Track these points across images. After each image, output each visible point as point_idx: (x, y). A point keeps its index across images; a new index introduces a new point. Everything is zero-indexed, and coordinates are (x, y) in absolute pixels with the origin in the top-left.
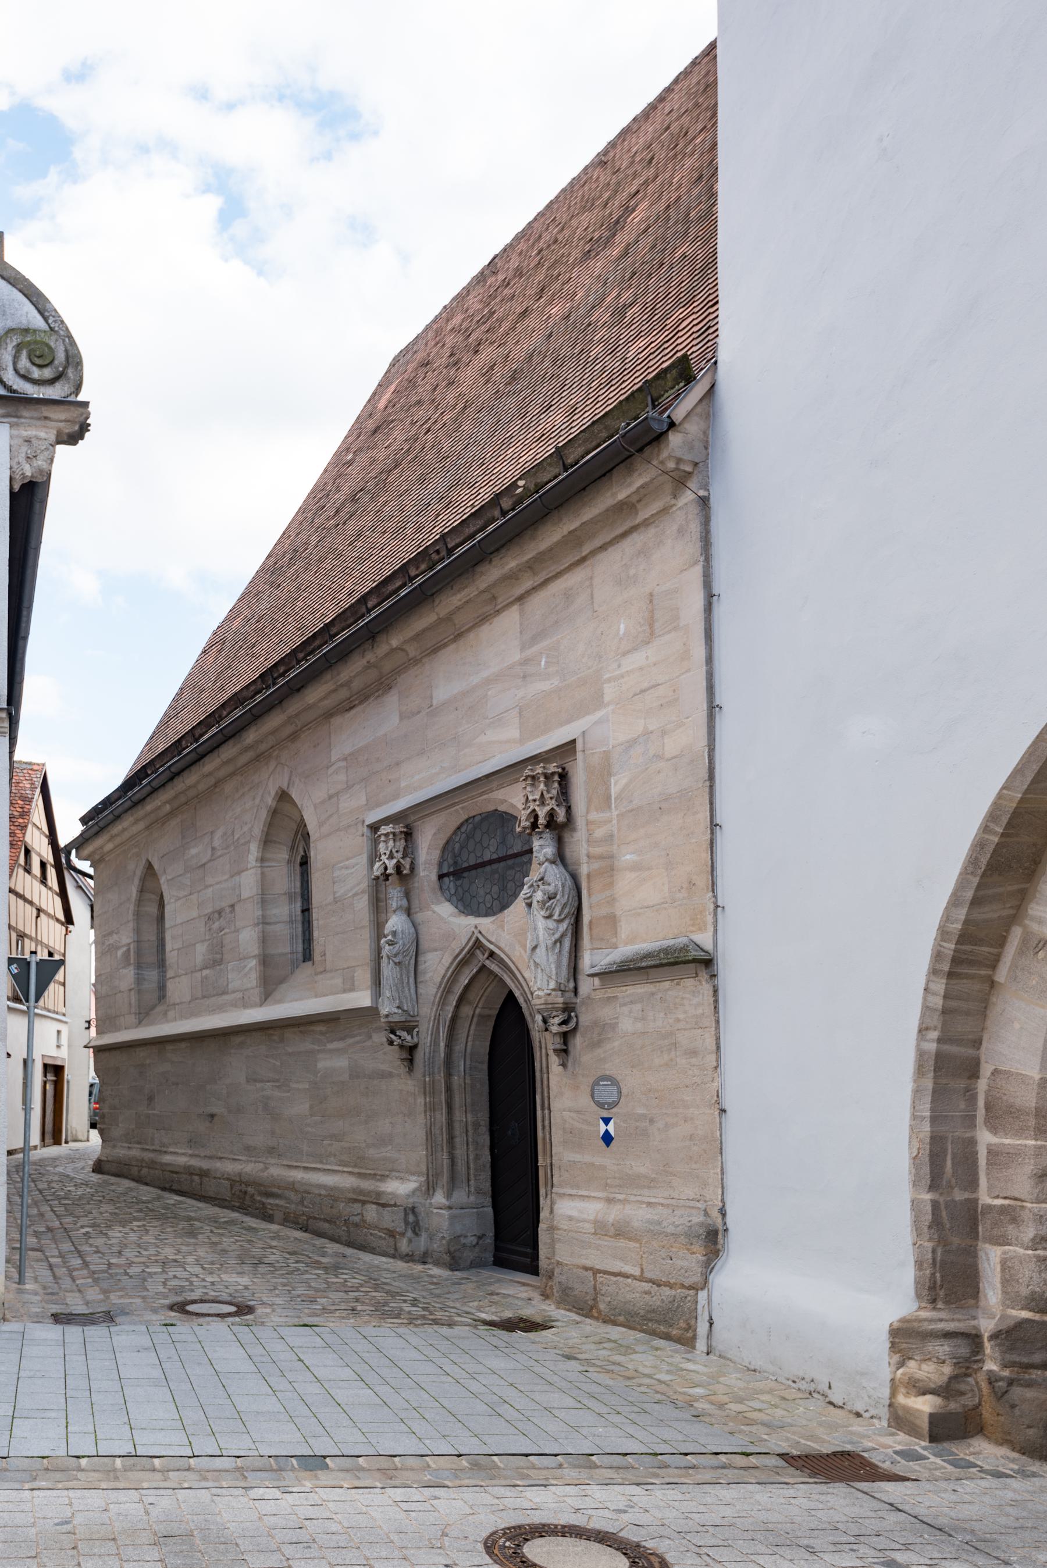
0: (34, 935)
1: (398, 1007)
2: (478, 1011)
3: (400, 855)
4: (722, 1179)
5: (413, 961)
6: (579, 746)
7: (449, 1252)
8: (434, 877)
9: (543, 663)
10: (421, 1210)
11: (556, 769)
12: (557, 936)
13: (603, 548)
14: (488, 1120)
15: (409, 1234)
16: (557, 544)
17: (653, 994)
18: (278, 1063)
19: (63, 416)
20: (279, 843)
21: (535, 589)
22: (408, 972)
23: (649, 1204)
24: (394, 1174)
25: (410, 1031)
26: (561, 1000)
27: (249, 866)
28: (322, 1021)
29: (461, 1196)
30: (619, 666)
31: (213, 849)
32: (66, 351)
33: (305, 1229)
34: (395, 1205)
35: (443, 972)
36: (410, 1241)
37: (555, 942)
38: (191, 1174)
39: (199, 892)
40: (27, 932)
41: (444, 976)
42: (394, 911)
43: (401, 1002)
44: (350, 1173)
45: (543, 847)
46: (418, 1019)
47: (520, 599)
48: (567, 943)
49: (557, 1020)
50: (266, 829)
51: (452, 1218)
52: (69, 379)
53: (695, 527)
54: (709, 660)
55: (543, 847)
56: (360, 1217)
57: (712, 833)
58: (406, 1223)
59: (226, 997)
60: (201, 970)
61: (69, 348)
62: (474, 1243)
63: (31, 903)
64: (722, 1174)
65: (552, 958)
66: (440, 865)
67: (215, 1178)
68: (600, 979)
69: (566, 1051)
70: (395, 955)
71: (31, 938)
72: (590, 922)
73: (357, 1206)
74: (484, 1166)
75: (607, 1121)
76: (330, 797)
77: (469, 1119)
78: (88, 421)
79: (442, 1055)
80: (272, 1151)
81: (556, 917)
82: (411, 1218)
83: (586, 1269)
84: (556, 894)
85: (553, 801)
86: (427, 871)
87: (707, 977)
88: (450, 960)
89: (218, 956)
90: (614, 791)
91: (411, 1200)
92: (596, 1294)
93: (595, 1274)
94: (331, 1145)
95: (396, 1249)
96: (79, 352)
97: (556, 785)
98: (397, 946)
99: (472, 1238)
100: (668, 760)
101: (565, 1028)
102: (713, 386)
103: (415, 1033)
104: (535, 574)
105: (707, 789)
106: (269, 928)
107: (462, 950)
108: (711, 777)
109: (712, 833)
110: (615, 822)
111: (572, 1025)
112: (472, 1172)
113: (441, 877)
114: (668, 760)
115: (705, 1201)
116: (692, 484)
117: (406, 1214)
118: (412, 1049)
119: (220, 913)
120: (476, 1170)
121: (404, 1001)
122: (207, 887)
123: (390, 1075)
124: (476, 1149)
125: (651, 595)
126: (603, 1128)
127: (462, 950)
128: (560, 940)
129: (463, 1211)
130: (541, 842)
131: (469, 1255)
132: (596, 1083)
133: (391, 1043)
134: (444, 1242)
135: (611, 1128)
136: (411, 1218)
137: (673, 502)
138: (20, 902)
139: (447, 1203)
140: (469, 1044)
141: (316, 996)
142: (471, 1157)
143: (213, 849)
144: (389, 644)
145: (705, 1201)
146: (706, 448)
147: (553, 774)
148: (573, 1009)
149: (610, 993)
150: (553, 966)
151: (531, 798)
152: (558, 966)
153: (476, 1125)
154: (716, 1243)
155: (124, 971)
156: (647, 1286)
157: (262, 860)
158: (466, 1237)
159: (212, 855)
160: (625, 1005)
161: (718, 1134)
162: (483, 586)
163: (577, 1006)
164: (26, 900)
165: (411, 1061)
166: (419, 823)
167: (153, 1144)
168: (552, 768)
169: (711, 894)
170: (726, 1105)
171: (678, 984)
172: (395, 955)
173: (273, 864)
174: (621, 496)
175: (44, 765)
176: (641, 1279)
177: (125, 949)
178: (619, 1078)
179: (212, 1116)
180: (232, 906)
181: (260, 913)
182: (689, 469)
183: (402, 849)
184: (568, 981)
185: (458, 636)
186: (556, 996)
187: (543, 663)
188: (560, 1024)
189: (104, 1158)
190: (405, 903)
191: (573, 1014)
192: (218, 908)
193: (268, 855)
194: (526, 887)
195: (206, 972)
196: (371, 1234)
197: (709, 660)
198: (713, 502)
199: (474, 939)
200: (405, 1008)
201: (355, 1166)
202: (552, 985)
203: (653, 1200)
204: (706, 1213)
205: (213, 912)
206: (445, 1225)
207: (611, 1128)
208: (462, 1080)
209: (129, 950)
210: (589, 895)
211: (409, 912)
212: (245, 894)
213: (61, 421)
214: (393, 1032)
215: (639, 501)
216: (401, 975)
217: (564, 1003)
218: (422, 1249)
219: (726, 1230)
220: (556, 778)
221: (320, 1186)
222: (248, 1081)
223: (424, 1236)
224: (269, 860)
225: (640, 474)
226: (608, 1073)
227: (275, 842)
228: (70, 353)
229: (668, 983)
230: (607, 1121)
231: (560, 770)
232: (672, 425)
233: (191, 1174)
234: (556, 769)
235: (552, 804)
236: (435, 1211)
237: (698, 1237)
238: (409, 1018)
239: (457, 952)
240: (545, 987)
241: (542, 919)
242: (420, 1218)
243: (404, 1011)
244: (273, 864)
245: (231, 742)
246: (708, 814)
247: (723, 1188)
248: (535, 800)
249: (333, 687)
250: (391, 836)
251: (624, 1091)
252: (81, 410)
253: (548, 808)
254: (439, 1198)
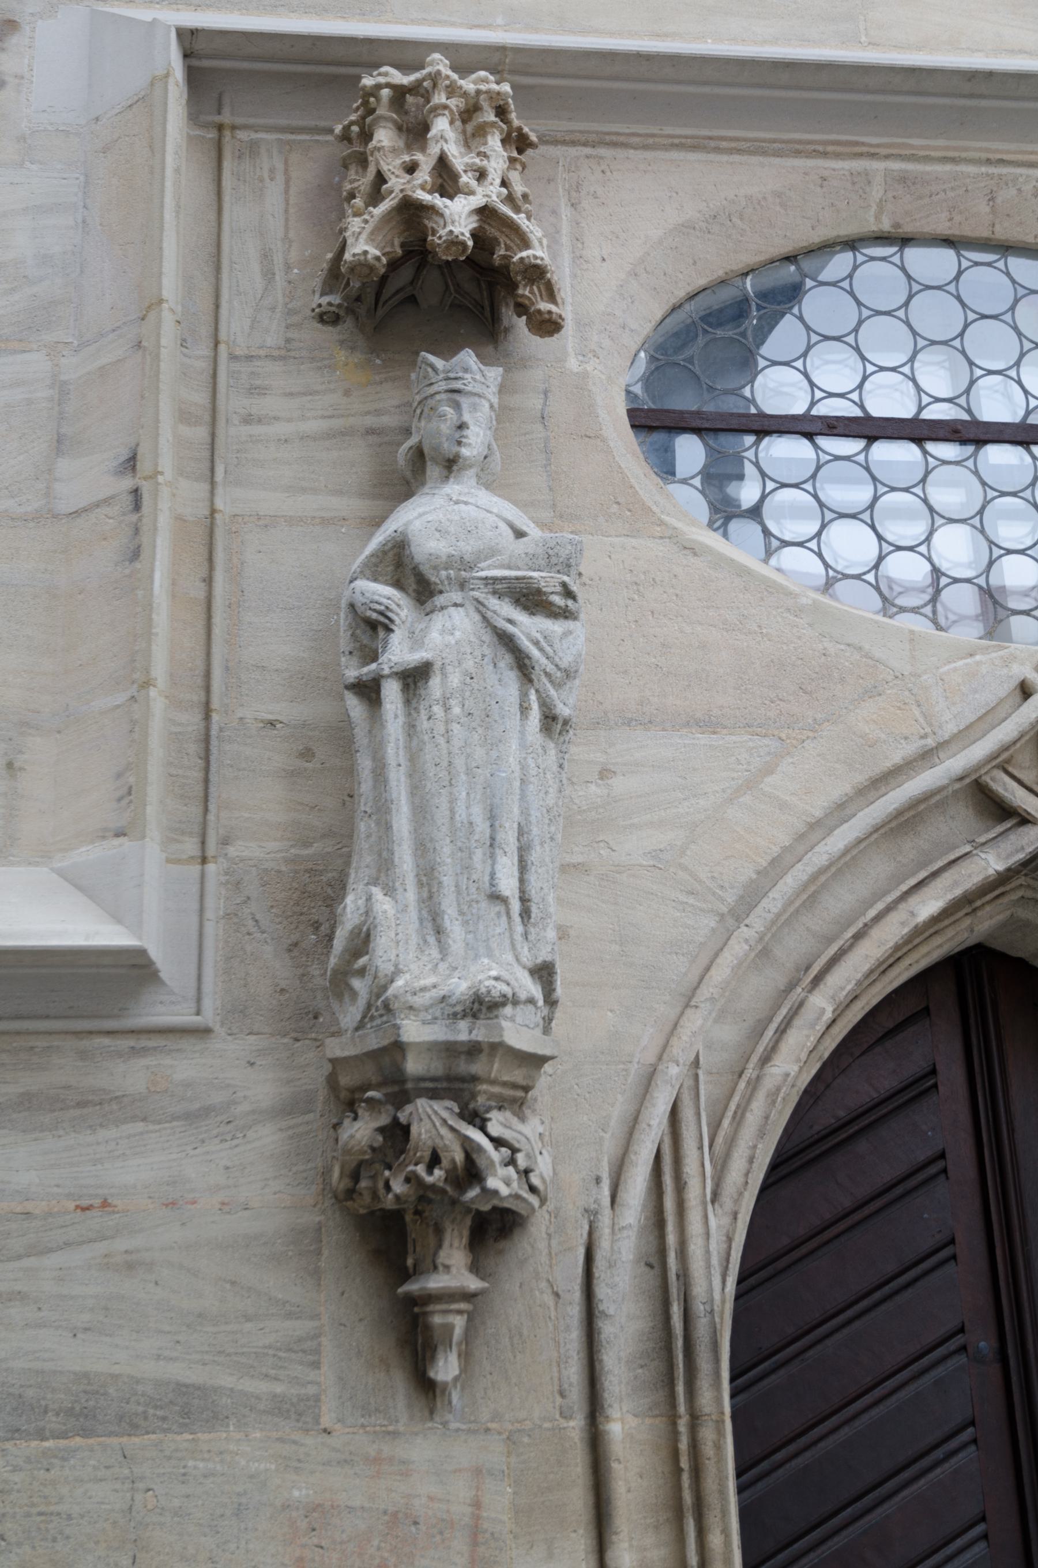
1: (544, 973)
41: (776, 867)
88: (841, 788)
107: (926, 756)
123: (190, 1408)
127: (926, 756)
239: (897, 756)
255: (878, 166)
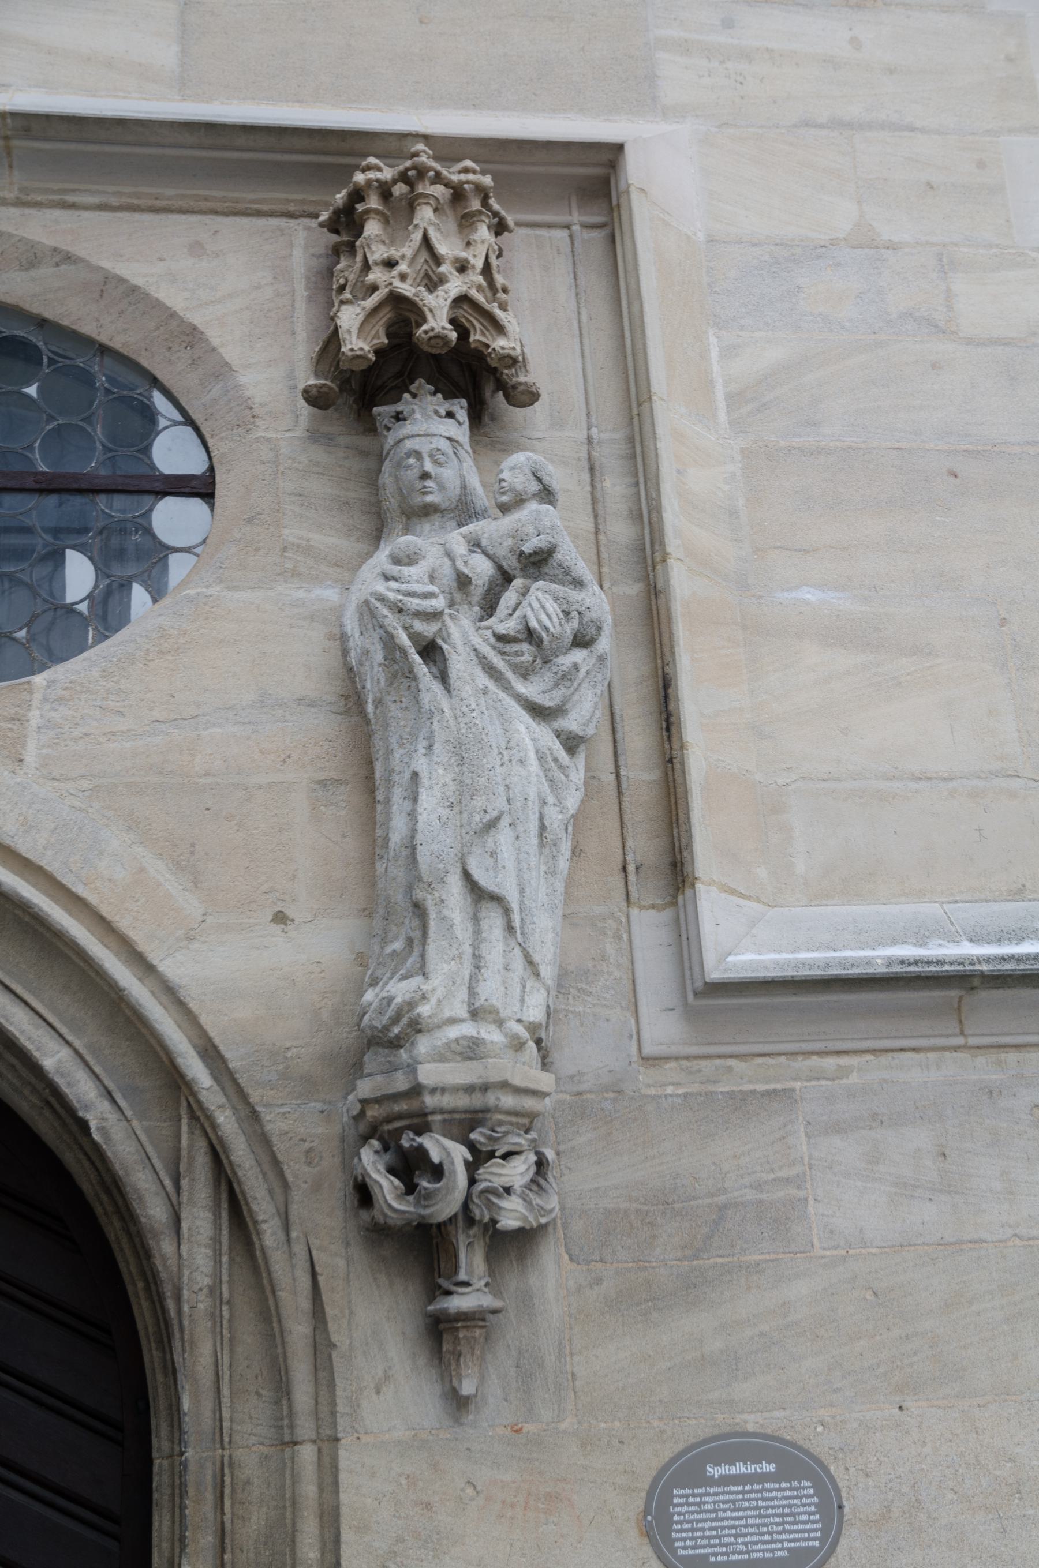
41: (144, 966)
100: (969, 341)
114: (969, 341)
130: (449, 428)
132: (687, 1469)
149: (746, 1077)
160: (838, 1128)
178: (821, 1443)
226: (751, 1422)
251: (859, 1499)
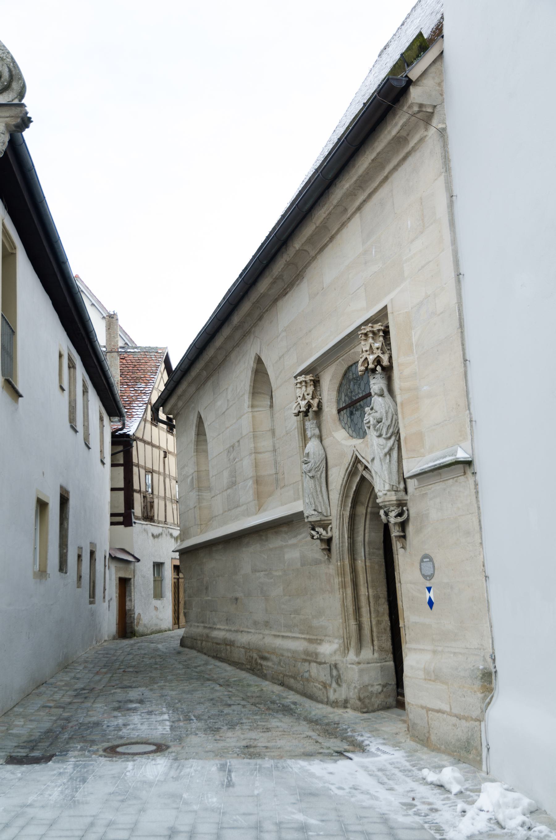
0: (162, 470)
1: (315, 510)
2: (369, 510)
3: (310, 397)
4: (491, 631)
5: (324, 475)
6: (389, 310)
7: (360, 699)
8: (335, 411)
9: (373, 252)
10: (340, 665)
11: (380, 327)
12: (386, 450)
13: (395, 168)
14: (386, 593)
15: (334, 685)
16: (368, 168)
17: (445, 490)
18: (266, 557)
19: (7, 114)
20: (263, 393)
21: (365, 201)
22: (320, 484)
23: (455, 653)
24: (327, 638)
25: (325, 528)
26: (394, 498)
27: (245, 412)
28: (285, 523)
29: (367, 653)
30: (410, 251)
31: (228, 400)
32: (10, 71)
33: (282, 684)
34: (325, 663)
35: (341, 482)
36: (335, 691)
37: (386, 455)
38: (226, 645)
39: (223, 432)
40: (156, 468)
41: (342, 485)
42: (310, 438)
43: (316, 506)
44: (304, 639)
45: (377, 384)
46: (330, 518)
47: (359, 208)
48: (395, 454)
49: (392, 514)
50: (252, 384)
51: (361, 671)
52: (13, 89)
53: (438, 150)
54: (454, 242)
55: (377, 384)
56: (308, 673)
57: (465, 366)
58: (332, 676)
59: (239, 509)
60: (226, 490)
61: (13, 69)
62: (380, 690)
63: (159, 447)
64: (491, 627)
65: (385, 467)
66: (338, 402)
67: (238, 647)
68: (418, 480)
69: (404, 537)
70: (310, 471)
71: (159, 473)
72: (405, 438)
73: (306, 664)
74: (385, 629)
75: (429, 589)
76: (280, 358)
77: (371, 593)
78: (28, 115)
79: (347, 545)
80: (267, 624)
81: (384, 436)
82: (335, 673)
83: (423, 707)
84: (382, 419)
85: (379, 351)
86: (330, 409)
87: (471, 474)
89: (234, 479)
90: (414, 340)
91: (334, 658)
92: (429, 728)
93: (427, 712)
94: (295, 618)
95: (328, 698)
96: (20, 72)
97: (381, 339)
98: (310, 464)
99: (377, 687)
101: (400, 520)
102: (442, 52)
103: (329, 529)
104: (364, 190)
105: (459, 334)
106: (260, 456)
107: (349, 464)
108: (461, 326)
109: (465, 366)
110: (416, 363)
111: (405, 516)
112: (375, 634)
113: (339, 411)
115: (484, 649)
116: (435, 122)
117: (331, 670)
118: (329, 541)
119: (233, 447)
120: (378, 633)
121: (318, 505)
122: (227, 428)
124: (377, 616)
125: (421, 199)
126: (428, 595)
128: (389, 453)
129: (369, 665)
131: (377, 702)
133: (312, 537)
134: (356, 690)
135: (432, 595)
136: (335, 673)
137: (426, 133)
138: (148, 447)
139: (357, 660)
140: (367, 535)
141: (282, 505)
142: (374, 623)
143: (228, 400)
144: (295, 247)
145: (484, 649)
146: (442, 95)
147: (379, 330)
148: (405, 505)
150: (386, 473)
151: (364, 349)
152: (390, 473)
153: (377, 598)
154: (491, 682)
155: (191, 493)
156: (454, 720)
157: (252, 406)
158: (372, 686)
159: (228, 405)
161: (486, 595)
162: (335, 202)
163: (408, 502)
164: (153, 446)
165: (329, 550)
166: (322, 373)
167: (209, 623)
168: (377, 327)
169: (468, 412)
170: (488, 573)
171: (456, 481)
172: (310, 471)
173: (260, 409)
174: (394, 132)
175: (167, 348)
176: (450, 714)
177: (191, 477)
179: (237, 599)
180: (239, 441)
181: (252, 445)
182: (430, 110)
183: (311, 393)
184: (399, 483)
185: (332, 238)
186: (391, 495)
187: (373, 252)
188: (396, 517)
189: (185, 635)
190: (317, 431)
191: (405, 508)
192: (232, 444)
193: (256, 403)
194: (366, 415)
195: (229, 491)
196: (315, 686)
197: (454, 242)
198: (450, 132)
199: (354, 456)
200: (320, 511)
201: (308, 633)
202: (387, 487)
203: (457, 651)
204: (485, 660)
205: (230, 447)
206: (356, 677)
207: (432, 595)
208: (363, 563)
209: (193, 477)
210: (403, 418)
211: (321, 438)
212: (244, 433)
213: (7, 117)
214: (313, 529)
215: (408, 135)
216: (315, 486)
217: (397, 500)
218: (344, 697)
219: (496, 672)
220: (381, 334)
221: (288, 650)
222: (252, 572)
223: (344, 686)
224: (257, 406)
225: (400, 117)
227: (260, 393)
228: (14, 73)
229: (451, 480)
230: (429, 589)
231: (383, 328)
232: (410, 82)
233: (226, 645)
234: (380, 327)
235: (379, 353)
236: (349, 666)
237: (476, 678)
238: (324, 518)
240: (382, 489)
241: (375, 438)
242: (341, 672)
243: (318, 512)
244: (260, 409)
245: (226, 324)
246: (461, 353)
247: (492, 638)
248: (367, 351)
249: (271, 280)
250: (304, 384)
251: (436, 565)
252: (19, 109)
253: (375, 356)
254: (352, 656)
255: (340, 360)
